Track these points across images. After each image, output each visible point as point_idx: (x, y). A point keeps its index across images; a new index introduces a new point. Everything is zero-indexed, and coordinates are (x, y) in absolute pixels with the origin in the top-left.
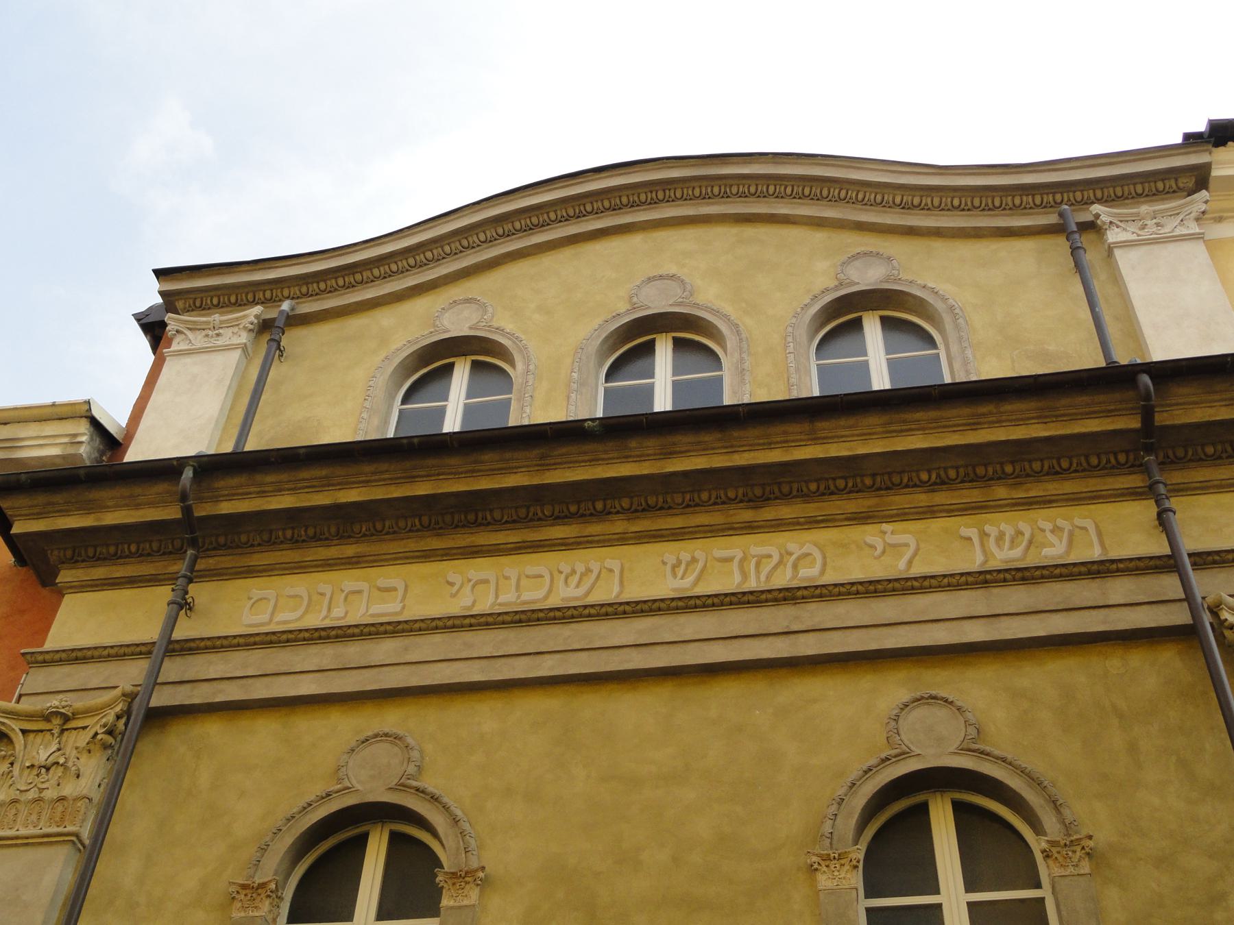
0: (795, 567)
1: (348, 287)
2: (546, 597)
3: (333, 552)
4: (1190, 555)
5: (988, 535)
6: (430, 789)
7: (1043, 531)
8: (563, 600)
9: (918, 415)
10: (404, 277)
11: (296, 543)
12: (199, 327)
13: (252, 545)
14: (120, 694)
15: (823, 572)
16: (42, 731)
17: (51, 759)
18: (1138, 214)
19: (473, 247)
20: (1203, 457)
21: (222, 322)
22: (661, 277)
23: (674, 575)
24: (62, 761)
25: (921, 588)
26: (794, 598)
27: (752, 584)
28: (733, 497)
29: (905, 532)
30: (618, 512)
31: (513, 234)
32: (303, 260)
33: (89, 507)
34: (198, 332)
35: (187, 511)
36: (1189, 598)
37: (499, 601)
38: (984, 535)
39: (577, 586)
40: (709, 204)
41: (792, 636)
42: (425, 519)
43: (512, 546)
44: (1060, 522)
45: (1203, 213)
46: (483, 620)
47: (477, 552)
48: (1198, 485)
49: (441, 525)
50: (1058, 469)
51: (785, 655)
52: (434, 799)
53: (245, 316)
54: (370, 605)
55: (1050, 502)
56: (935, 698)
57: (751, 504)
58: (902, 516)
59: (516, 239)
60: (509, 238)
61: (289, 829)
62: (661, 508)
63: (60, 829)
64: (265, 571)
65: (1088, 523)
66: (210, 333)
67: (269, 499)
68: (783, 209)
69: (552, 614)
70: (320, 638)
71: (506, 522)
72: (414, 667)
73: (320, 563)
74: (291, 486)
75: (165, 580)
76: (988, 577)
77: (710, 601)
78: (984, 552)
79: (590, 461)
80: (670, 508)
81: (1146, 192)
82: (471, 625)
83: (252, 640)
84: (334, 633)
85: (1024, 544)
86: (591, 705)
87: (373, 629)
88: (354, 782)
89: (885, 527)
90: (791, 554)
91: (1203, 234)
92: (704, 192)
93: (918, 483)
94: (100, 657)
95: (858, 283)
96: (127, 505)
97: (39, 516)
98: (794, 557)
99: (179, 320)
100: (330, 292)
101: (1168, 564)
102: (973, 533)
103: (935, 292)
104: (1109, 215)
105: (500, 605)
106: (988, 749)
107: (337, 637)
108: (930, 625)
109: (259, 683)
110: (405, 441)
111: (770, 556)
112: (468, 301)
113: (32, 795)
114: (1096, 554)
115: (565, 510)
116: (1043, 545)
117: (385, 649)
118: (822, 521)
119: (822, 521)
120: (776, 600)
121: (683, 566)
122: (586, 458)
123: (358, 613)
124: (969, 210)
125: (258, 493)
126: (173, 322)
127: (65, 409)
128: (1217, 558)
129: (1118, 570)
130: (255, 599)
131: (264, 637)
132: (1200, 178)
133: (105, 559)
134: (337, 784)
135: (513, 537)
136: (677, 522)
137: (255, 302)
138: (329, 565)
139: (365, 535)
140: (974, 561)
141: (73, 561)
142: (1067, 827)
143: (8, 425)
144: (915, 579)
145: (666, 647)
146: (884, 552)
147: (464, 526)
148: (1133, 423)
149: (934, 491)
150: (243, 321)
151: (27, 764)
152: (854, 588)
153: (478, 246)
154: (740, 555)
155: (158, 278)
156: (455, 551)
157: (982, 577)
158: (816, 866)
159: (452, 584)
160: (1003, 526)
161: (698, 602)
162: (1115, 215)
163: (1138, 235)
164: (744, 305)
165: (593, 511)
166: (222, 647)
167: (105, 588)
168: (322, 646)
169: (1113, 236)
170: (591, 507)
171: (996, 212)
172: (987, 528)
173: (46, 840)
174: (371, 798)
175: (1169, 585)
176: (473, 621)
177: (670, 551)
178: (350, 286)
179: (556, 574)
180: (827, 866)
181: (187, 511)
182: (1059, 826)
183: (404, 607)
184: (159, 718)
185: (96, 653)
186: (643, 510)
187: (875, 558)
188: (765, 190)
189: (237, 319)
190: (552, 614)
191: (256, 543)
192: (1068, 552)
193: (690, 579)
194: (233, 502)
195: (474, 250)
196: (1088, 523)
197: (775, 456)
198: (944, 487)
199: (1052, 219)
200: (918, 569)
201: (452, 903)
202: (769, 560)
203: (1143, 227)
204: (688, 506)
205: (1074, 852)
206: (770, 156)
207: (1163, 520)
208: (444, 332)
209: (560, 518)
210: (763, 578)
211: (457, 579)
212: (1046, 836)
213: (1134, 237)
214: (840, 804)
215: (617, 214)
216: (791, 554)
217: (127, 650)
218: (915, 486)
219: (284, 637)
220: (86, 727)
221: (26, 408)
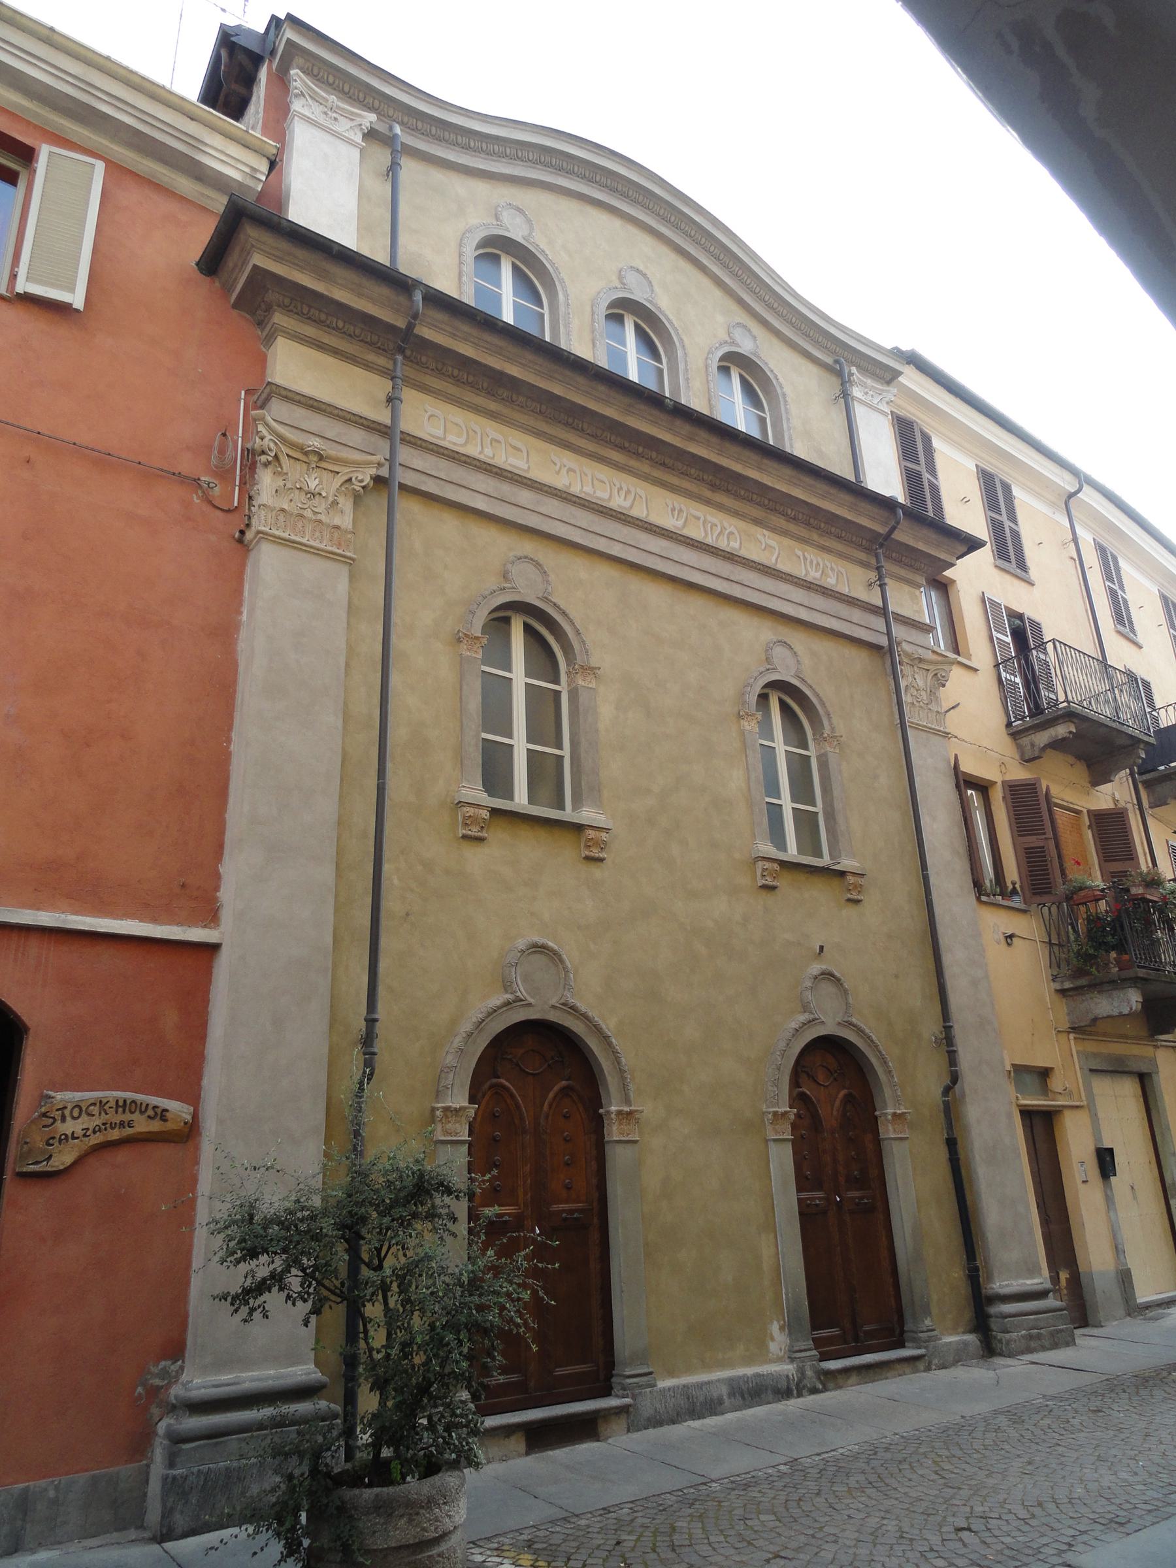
3: (480, 400)
11: (458, 381)
12: (317, 99)
13: (427, 368)
14: (376, 461)
16: (299, 460)
18: (865, 383)
26: (732, 560)
28: (305, 312)
30: (647, 459)
33: (323, 276)
35: (410, 327)
36: (889, 633)
40: (664, 225)
41: (730, 582)
42: (544, 407)
45: (891, 401)
47: (568, 447)
56: (785, 643)
60: (544, 168)
64: (434, 393)
68: (705, 261)
70: (486, 470)
71: (588, 434)
74: (476, 341)
79: (652, 421)
82: (575, 502)
83: (442, 450)
94: (330, 413)
96: (352, 290)
97: (278, 259)
103: (776, 377)
104: (857, 376)
107: (496, 474)
108: (510, 506)
109: (449, 487)
110: (566, 354)
117: (525, 496)
120: (724, 557)
122: (651, 418)
125: (450, 333)
127: (176, 100)
129: (857, 605)
131: (382, 427)
135: (591, 446)
137: (371, 109)
138: (478, 410)
141: (287, 310)
142: (833, 729)
143: (194, 122)
148: (882, 530)
150: (358, 119)
161: (649, 527)
166: (421, 447)
173: (332, 556)
175: (880, 624)
176: (577, 500)
178: (439, 139)
181: (410, 327)
185: (329, 409)
189: (352, 113)
197: (737, 468)
199: (829, 360)
204: (682, 473)
207: (392, 400)
209: (620, 448)
215: (611, 195)
217: (353, 418)
221: (97, 53)
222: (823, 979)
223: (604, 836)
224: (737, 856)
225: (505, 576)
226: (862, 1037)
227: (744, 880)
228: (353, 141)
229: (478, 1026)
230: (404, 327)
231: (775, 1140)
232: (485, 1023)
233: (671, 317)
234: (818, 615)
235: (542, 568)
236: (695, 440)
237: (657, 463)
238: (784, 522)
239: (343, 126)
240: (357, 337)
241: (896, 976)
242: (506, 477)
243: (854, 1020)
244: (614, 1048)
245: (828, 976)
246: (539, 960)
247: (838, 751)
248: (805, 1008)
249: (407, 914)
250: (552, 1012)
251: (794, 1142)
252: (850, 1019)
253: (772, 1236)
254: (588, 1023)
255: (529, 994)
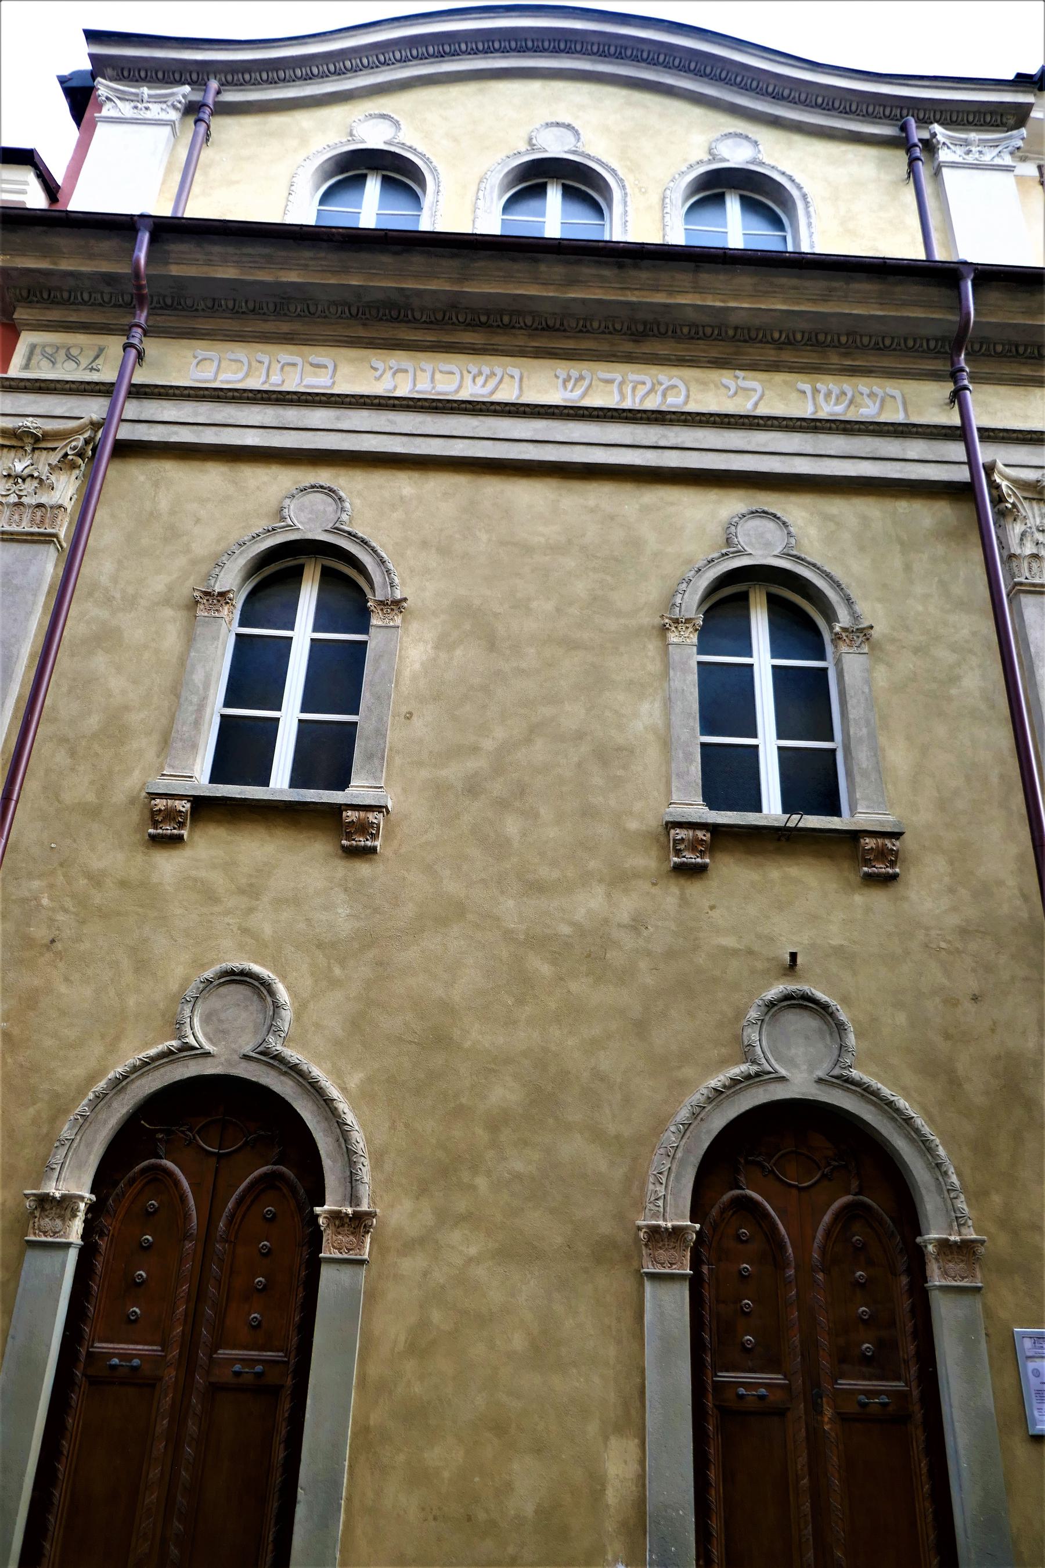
0: (664, 395)
1: (271, 83)
2: (457, 391)
3: (269, 327)
4: (979, 429)
5: (819, 391)
6: (360, 534)
7: (862, 394)
8: (471, 395)
9: (784, 281)
10: (324, 82)
12: (127, 97)
13: (197, 310)
15: (686, 402)
17: (26, 472)
19: (388, 65)
20: (993, 353)
21: (150, 96)
22: (558, 124)
23: (565, 387)
24: (36, 474)
25: (765, 426)
27: (627, 404)
29: (754, 379)
30: (521, 328)
31: (426, 58)
32: (268, 45)
33: (46, 252)
34: (127, 103)
37: (416, 389)
38: (816, 391)
39: (483, 386)
43: (429, 343)
44: (875, 389)
45: (1018, 148)
46: (405, 402)
48: (985, 375)
49: (368, 316)
50: (882, 346)
51: (653, 464)
52: (364, 542)
53: (172, 94)
54: (303, 377)
55: (871, 372)
57: (633, 337)
58: (753, 367)
59: (428, 63)
60: (422, 62)
61: (241, 553)
62: (558, 330)
63: (42, 530)
65: (896, 393)
66: (139, 105)
67: (216, 268)
69: (463, 406)
71: (425, 322)
72: (344, 435)
73: (258, 334)
75: (116, 330)
76: (818, 424)
77: (595, 413)
78: (815, 404)
80: (565, 330)
81: (975, 122)
84: (274, 396)
85: (847, 402)
86: (493, 487)
87: (309, 398)
88: (296, 522)
89: (738, 373)
90: (661, 384)
91: (1014, 167)
92: (601, 49)
93: (770, 340)
95: (728, 161)
98: (664, 387)
99: (108, 87)
100: (254, 84)
101: (960, 433)
102: (807, 387)
104: (944, 135)
105: (417, 392)
106: (803, 556)
111: (644, 383)
112: (383, 116)
113: (13, 499)
114: (900, 417)
115: (476, 319)
116: (859, 406)
118: (688, 361)
119: (688, 361)
121: (572, 381)
123: (292, 383)
124: (829, 110)
126: (103, 87)
128: (991, 434)
130: (200, 358)
132: (1019, 115)
133: (58, 303)
134: (280, 521)
136: (570, 344)
137: (180, 82)
138: (266, 337)
139: (299, 316)
140: (806, 410)
142: (855, 617)
144: (762, 417)
145: (557, 446)
146: (736, 393)
147: (387, 320)
149: (781, 349)
151: (5, 474)
152: (712, 419)
153: (393, 64)
154: (620, 379)
155: (87, 38)
156: (379, 341)
157: (813, 424)
158: (668, 626)
159: (376, 369)
160: (831, 386)
161: (586, 412)
162: (950, 137)
163: (964, 159)
164: (629, 163)
165: (500, 323)
167: (60, 329)
168: (264, 406)
169: (944, 155)
170: (499, 320)
171: (851, 116)
172: (819, 385)
174: (310, 536)
175: (956, 451)
176: (396, 402)
177: (562, 368)
179: (465, 373)
180: (676, 627)
182: (849, 617)
183: (334, 383)
184: (125, 450)
186: (543, 329)
187: (729, 397)
188: (656, 57)
190: (463, 406)
191: (199, 308)
192: (879, 414)
193: (578, 393)
194: (181, 266)
195: (388, 67)
196: (896, 393)
198: (789, 347)
200: (763, 411)
201: (380, 623)
202: (644, 386)
203: (969, 152)
205: (858, 637)
206: (666, 24)
207: (957, 397)
208: (361, 142)
210: (637, 400)
211: (380, 365)
212: (839, 622)
213: (960, 160)
214: (688, 583)
216: (661, 384)
218: (768, 342)
219: (230, 394)
220: (55, 449)
222: (790, 1006)
223: (372, 817)
224: (633, 825)
225: (280, 513)
226: (874, 1104)
227: (647, 861)
228: (162, 120)
229: (117, 1085)
230: (130, 272)
231: (654, 1277)
232: (128, 1080)
233: (614, 165)
234: (835, 462)
235: (336, 494)
236: (579, 281)
237: (536, 329)
238: (773, 352)
239: (155, 111)
240: (108, 303)
241: (975, 999)
242: (292, 401)
243: (855, 1074)
244: (340, 1117)
245: (803, 1002)
246: (237, 992)
247: (866, 650)
248: (747, 1054)
249: (53, 941)
250: (244, 1064)
251: (696, 1283)
252: (845, 1072)
253: (632, 1445)
254: (301, 1080)
255: (210, 1040)
